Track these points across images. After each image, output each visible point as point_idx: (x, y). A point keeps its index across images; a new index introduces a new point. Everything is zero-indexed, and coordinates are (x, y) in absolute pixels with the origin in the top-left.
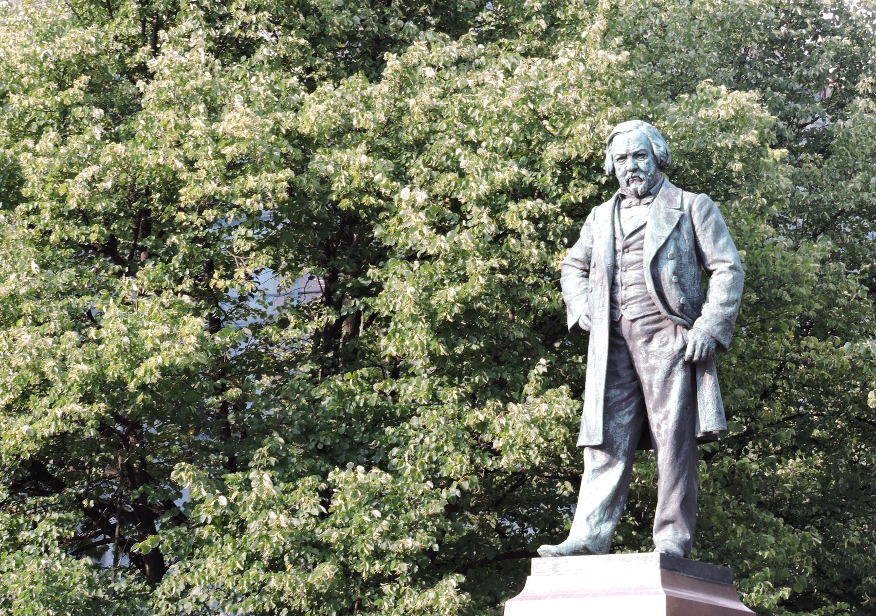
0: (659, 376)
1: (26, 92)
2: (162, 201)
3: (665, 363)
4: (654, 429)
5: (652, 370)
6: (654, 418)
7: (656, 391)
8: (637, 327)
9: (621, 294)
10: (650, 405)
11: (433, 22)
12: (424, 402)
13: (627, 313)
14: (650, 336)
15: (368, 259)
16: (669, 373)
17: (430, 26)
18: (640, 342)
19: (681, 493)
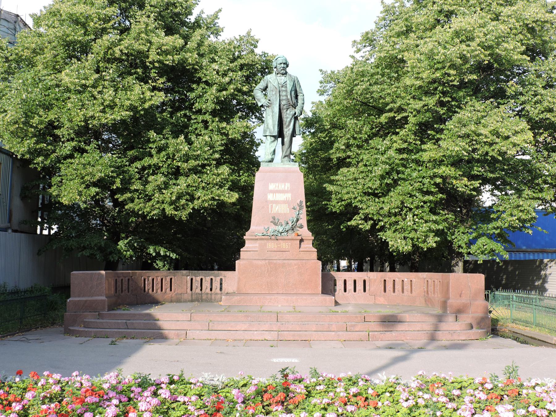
0: (289, 119)
1: (382, 154)
2: (270, 61)
3: (291, 116)
4: (285, 133)
5: (287, 118)
6: (285, 130)
7: (287, 123)
8: (285, 107)
9: (281, 98)
10: (285, 126)
11: (489, 157)
12: (163, 50)
13: (283, 103)
14: (287, 109)
15: (62, 225)
16: (291, 119)
17: (490, 156)
18: (285, 111)
19: (399, 326)
